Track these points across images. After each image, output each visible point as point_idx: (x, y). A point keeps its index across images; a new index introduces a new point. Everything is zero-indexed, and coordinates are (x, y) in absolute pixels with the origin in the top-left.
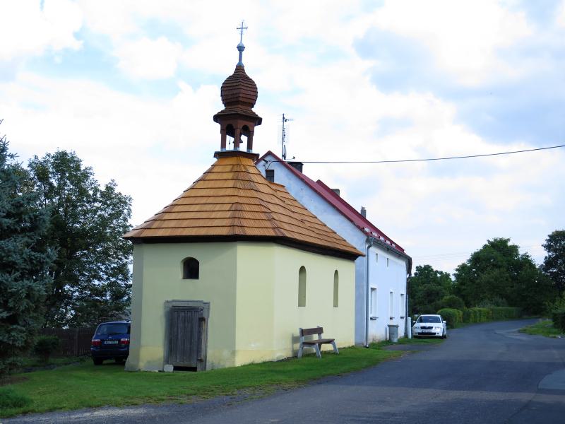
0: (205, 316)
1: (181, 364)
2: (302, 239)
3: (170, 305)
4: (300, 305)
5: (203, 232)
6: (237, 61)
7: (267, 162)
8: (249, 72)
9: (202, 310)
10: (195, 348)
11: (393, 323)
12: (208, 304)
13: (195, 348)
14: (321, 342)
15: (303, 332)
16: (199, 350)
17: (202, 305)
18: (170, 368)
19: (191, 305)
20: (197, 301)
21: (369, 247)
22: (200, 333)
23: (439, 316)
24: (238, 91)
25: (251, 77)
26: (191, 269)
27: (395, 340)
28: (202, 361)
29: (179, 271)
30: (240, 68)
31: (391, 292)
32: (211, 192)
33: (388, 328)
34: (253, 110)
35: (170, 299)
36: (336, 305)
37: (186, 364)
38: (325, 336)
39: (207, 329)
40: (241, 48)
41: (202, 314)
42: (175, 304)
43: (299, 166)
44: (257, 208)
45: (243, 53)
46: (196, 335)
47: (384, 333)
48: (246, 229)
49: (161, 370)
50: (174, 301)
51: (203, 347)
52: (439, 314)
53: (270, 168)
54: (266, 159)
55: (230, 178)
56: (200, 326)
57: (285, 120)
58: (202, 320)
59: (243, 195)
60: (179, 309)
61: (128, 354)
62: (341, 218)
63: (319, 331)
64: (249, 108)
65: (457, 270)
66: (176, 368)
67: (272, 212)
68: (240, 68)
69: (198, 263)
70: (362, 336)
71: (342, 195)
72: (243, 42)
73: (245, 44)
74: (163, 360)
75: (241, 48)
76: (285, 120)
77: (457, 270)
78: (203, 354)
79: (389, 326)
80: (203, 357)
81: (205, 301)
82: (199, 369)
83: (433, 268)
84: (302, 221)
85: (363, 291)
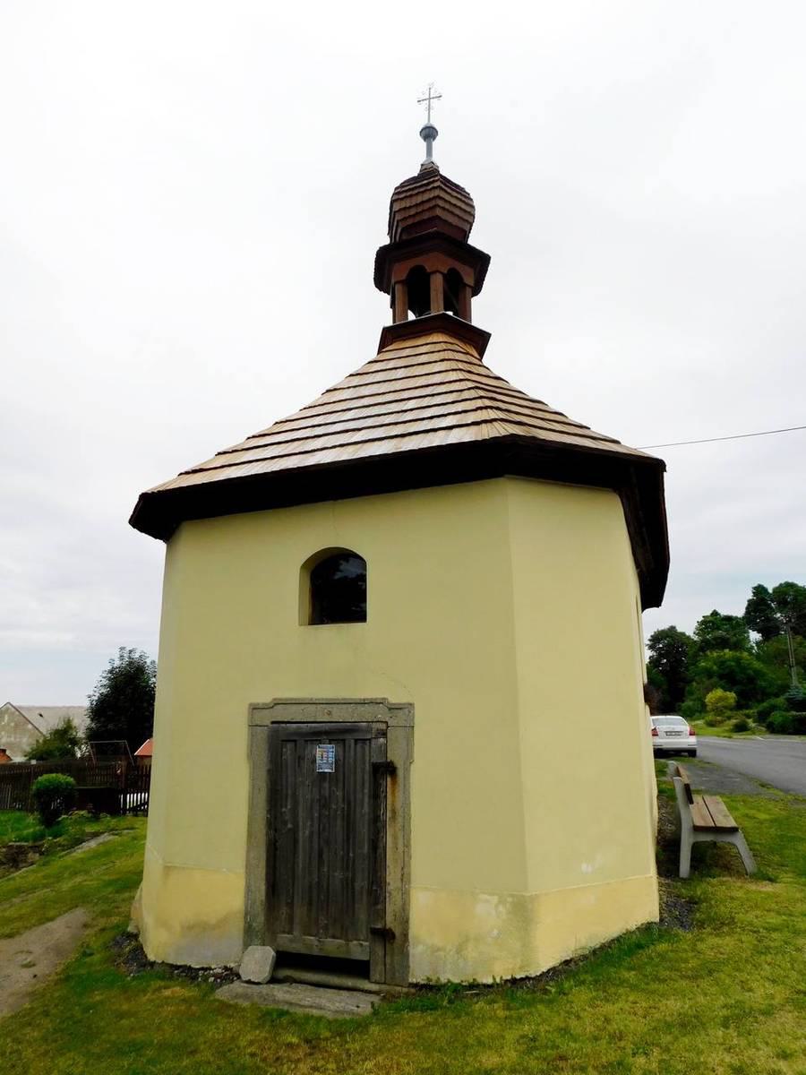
0: (394, 756)
3: (266, 718)
9: (384, 734)
10: (361, 883)
13: (361, 883)
17: (382, 714)
18: (257, 962)
20: (363, 703)
28: (390, 938)
29: (290, 591)
32: (401, 373)
35: (265, 698)
37: (332, 946)
39: (407, 805)
40: (429, 134)
41: (384, 750)
42: (282, 714)
45: (435, 144)
46: (363, 831)
50: (277, 703)
56: (377, 796)
58: (385, 771)
60: (299, 734)
61: (141, 880)
65: (650, 640)
66: (284, 960)
72: (431, 122)
75: (429, 134)
77: (650, 640)
78: (391, 908)
80: (390, 921)
81: (394, 699)
82: (376, 972)
83: (677, 628)
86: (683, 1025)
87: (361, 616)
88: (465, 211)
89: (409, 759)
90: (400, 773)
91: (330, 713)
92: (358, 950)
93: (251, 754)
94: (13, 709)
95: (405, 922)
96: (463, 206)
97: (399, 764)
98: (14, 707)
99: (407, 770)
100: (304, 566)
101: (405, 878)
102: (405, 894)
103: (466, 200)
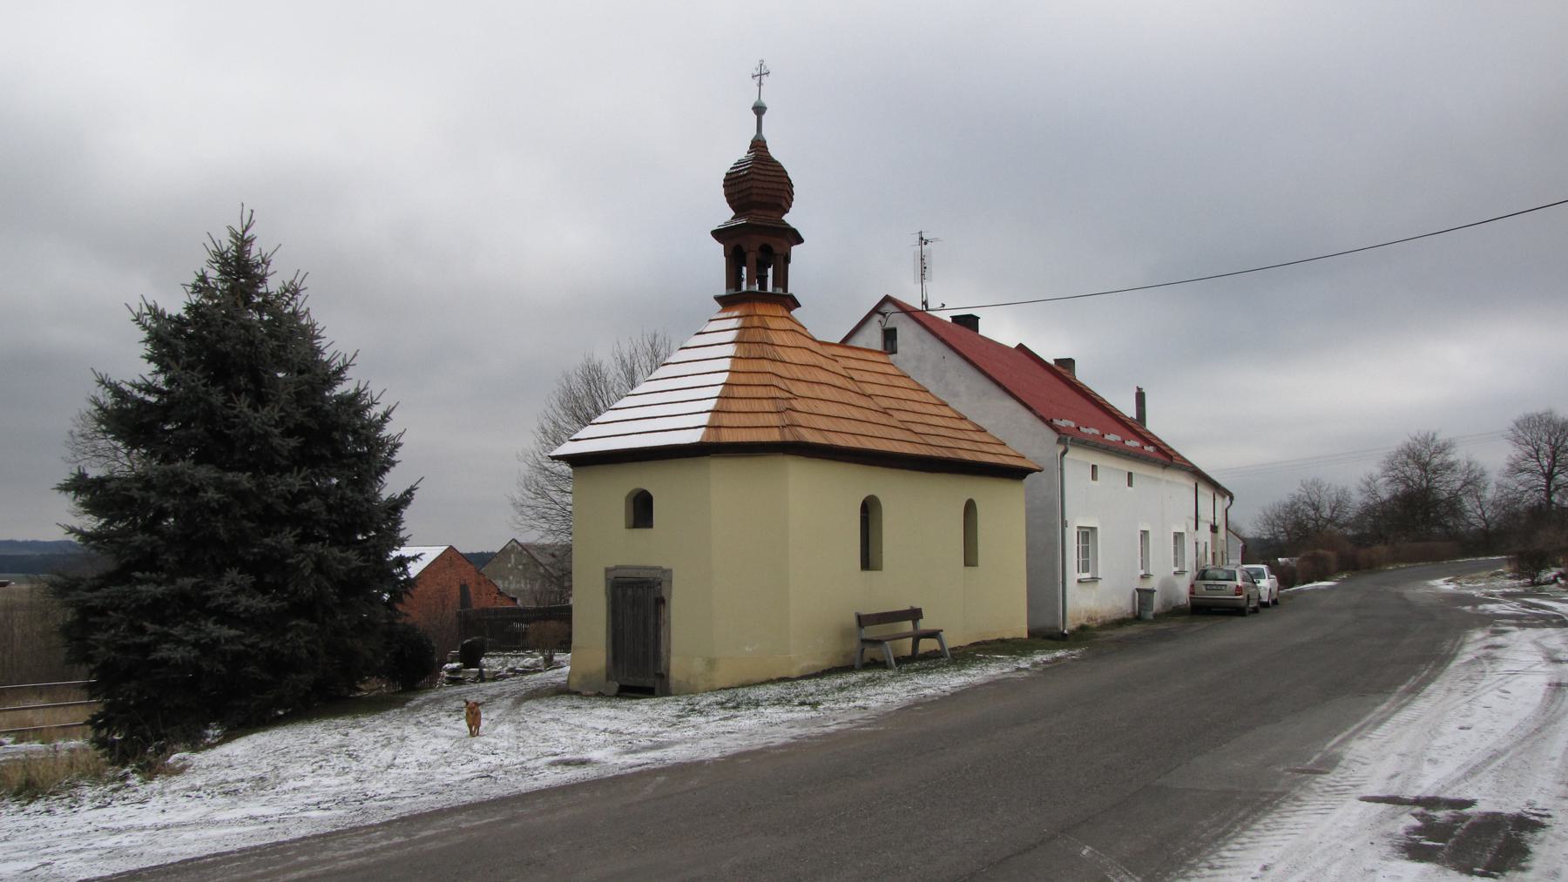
0: (664, 594)
1: (631, 682)
2: (858, 445)
3: (612, 575)
4: (967, 564)
5: (852, 442)
6: (754, 133)
7: (884, 315)
8: (775, 152)
9: (660, 584)
11: (1147, 585)
12: (668, 572)
14: (917, 637)
15: (863, 620)
16: (657, 657)
19: (643, 574)
21: (1063, 454)
22: (657, 627)
23: (1264, 567)
24: (749, 185)
25: (776, 158)
26: (641, 510)
27: (1150, 615)
30: (758, 145)
31: (1145, 534)
33: (1137, 594)
34: (787, 218)
35: (611, 565)
36: (970, 559)
38: (925, 624)
40: (759, 110)
43: (970, 322)
44: (762, 392)
45: (764, 118)
47: (1130, 602)
48: (724, 431)
49: (1251, 597)
50: (616, 568)
51: (663, 651)
52: (1264, 564)
53: (889, 325)
54: (882, 310)
55: (729, 341)
56: (657, 614)
57: (923, 241)
58: (661, 602)
59: (742, 369)
62: (1011, 404)
63: (915, 614)
64: (775, 214)
67: (796, 397)
68: (758, 145)
69: (646, 491)
70: (1056, 615)
71: (1082, 375)
73: (765, 101)
74: (604, 673)
75: (759, 110)
76: (923, 241)
78: (663, 664)
79: (1138, 590)
80: (663, 670)
81: (665, 566)
84: (885, 412)
85: (1056, 534)
86: (209, 822)
87: (651, 526)
88: (780, 176)
89: (670, 595)
90: (667, 602)
91: (862, 376)
92: (649, 683)
93: (606, 593)
94: (520, 548)
95: (668, 670)
96: (778, 174)
97: (666, 598)
98: (521, 546)
99: (669, 601)
100: (627, 498)
101: (669, 651)
102: (669, 658)
103: (776, 169)
